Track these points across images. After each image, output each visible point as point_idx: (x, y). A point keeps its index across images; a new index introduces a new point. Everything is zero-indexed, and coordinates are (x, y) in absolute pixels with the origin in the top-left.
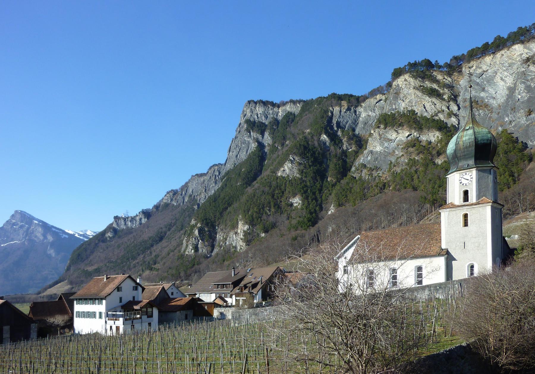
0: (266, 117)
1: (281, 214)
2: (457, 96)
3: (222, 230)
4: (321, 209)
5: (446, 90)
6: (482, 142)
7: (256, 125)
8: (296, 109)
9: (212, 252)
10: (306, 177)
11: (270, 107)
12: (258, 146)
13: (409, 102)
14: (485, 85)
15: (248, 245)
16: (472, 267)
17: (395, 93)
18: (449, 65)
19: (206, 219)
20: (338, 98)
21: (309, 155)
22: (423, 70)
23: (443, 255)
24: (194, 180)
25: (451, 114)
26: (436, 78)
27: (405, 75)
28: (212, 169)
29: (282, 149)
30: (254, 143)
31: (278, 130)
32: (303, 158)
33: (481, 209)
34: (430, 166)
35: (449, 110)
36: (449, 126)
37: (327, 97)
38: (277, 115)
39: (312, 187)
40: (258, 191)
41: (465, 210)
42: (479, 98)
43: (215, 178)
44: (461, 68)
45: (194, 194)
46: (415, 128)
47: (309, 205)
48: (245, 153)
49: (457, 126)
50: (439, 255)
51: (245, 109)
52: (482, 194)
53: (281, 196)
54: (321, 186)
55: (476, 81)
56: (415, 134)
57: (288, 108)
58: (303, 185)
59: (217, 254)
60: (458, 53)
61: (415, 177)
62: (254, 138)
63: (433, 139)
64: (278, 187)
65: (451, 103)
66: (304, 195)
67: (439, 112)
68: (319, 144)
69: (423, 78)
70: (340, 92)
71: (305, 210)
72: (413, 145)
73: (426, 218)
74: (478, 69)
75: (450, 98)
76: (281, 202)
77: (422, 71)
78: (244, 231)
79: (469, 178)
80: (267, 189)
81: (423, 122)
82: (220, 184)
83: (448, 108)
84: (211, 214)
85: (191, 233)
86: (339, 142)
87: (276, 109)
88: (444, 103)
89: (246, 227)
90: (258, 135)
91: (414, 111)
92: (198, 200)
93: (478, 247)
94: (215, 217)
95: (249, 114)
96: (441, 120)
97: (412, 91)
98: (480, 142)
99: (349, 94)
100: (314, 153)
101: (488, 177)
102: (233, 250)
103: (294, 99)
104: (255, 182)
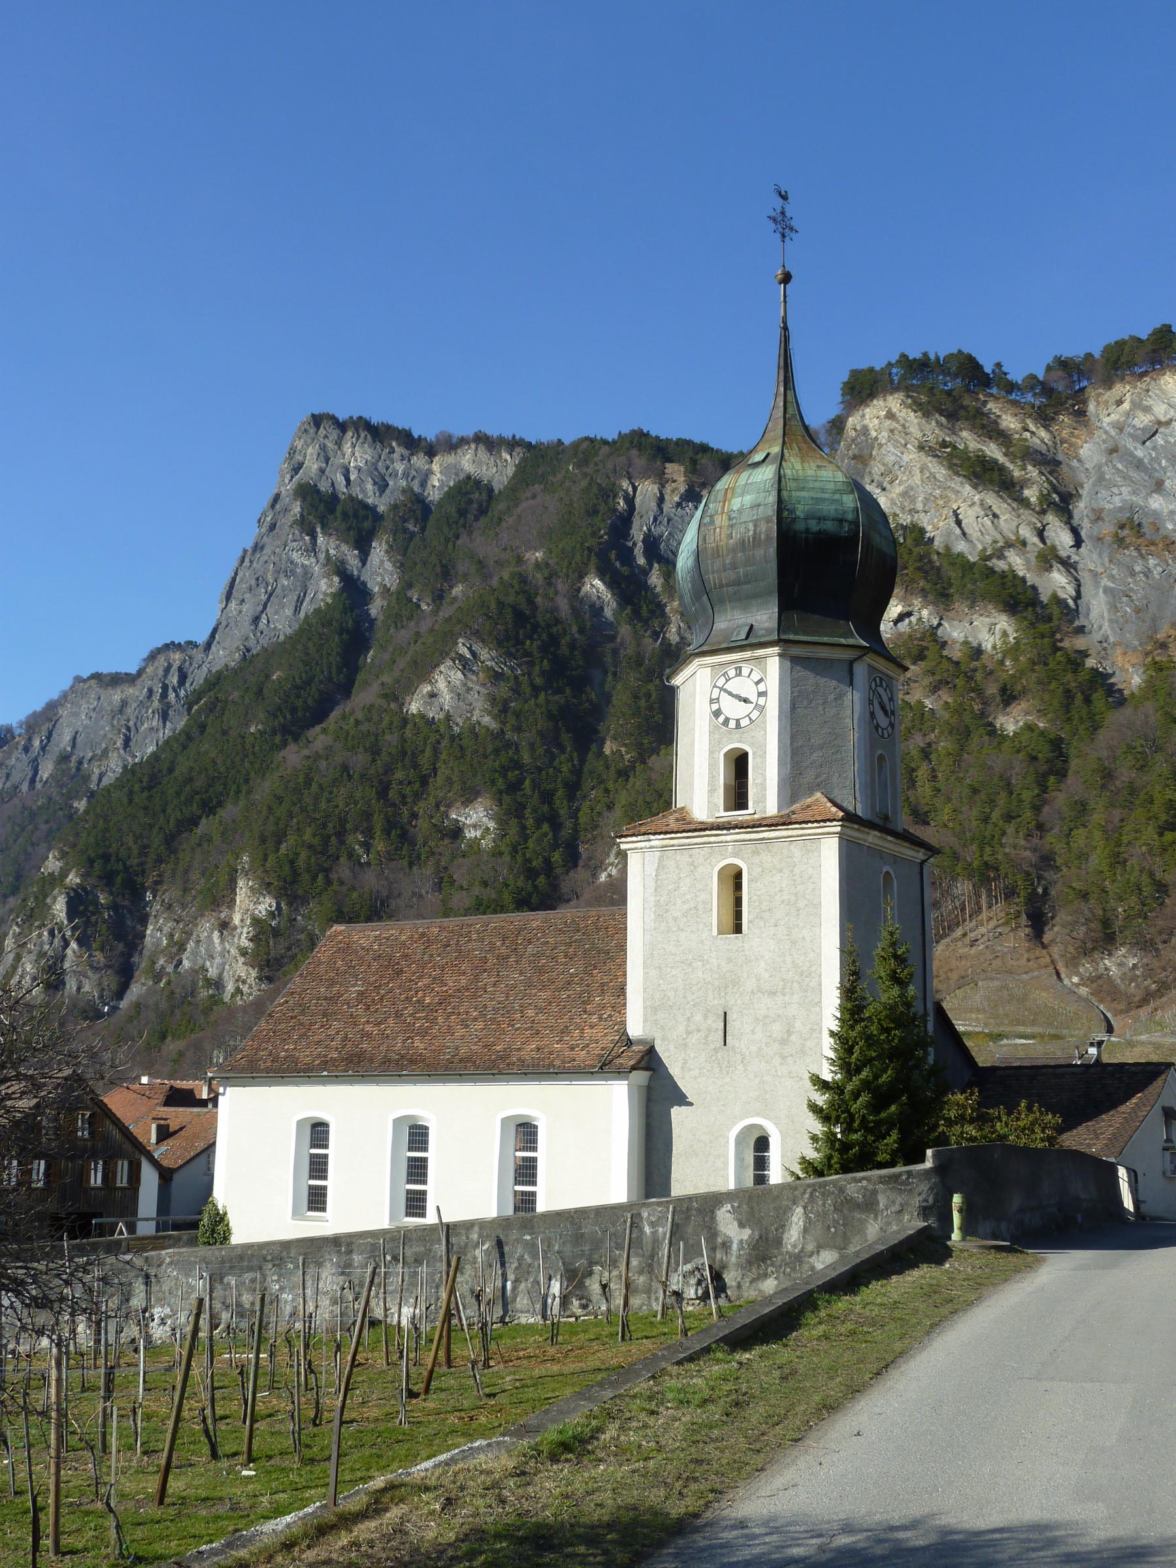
0: (382, 486)
1: (411, 865)
2: (1071, 495)
3: (170, 907)
4: (573, 859)
5: (1033, 472)
6: (814, 526)
7: (339, 508)
8: (498, 471)
9: (120, 994)
10: (518, 729)
11: (399, 450)
12: (342, 590)
13: (904, 494)
14: (1164, 469)
15: (270, 979)
16: (762, 1144)
17: (854, 457)
18: (1042, 383)
19: (106, 858)
20: (658, 452)
21: (532, 646)
22: (952, 387)
23: (621, 1073)
24: (84, 694)
25: (1049, 558)
26: (996, 423)
27: (890, 398)
28: (161, 661)
29: (435, 612)
30: (327, 575)
31: (423, 540)
32: (511, 655)
33: (796, 850)
34: (975, 739)
35: (1043, 540)
36: (1044, 598)
37: (614, 442)
38: (423, 484)
39: (540, 770)
40: (323, 764)
41: (729, 851)
42: (1146, 514)
43: (164, 695)
44: (1085, 402)
45: (79, 753)
46: (924, 593)
47: (526, 839)
48: (288, 612)
49: (1071, 602)
50: (604, 1068)
51: (299, 444)
52: (809, 777)
53: (417, 796)
54: (578, 772)
55: (1132, 455)
56: (925, 613)
57: (468, 461)
58: (504, 758)
59: (138, 1006)
60: (1074, 350)
61: (923, 772)
62: (328, 557)
63: (988, 642)
64: (406, 755)
65: (1050, 518)
66: (507, 799)
67: (1009, 545)
68: (573, 608)
69: (952, 416)
70: (665, 429)
71: (507, 858)
72: (915, 652)
73: (959, 932)
74: (1140, 414)
75: (1044, 498)
76: (414, 816)
77: (949, 393)
78: (256, 921)
79: (750, 692)
80: (360, 759)
81: (953, 574)
82: (179, 722)
83: (1041, 534)
84: (129, 840)
85: (35, 914)
86: (652, 612)
87: (419, 461)
88: (1026, 514)
89: (265, 905)
90: (344, 548)
91: (922, 531)
92: (95, 778)
93: (784, 1042)
94: (144, 850)
95: (312, 466)
96: (1015, 576)
97: (912, 456)
98: (800, 526)
99: (697, 440)
100: (554, 640)
101: (840, 697)
102: (204, 994)
103: (493, 431)
104: (318, 728)
